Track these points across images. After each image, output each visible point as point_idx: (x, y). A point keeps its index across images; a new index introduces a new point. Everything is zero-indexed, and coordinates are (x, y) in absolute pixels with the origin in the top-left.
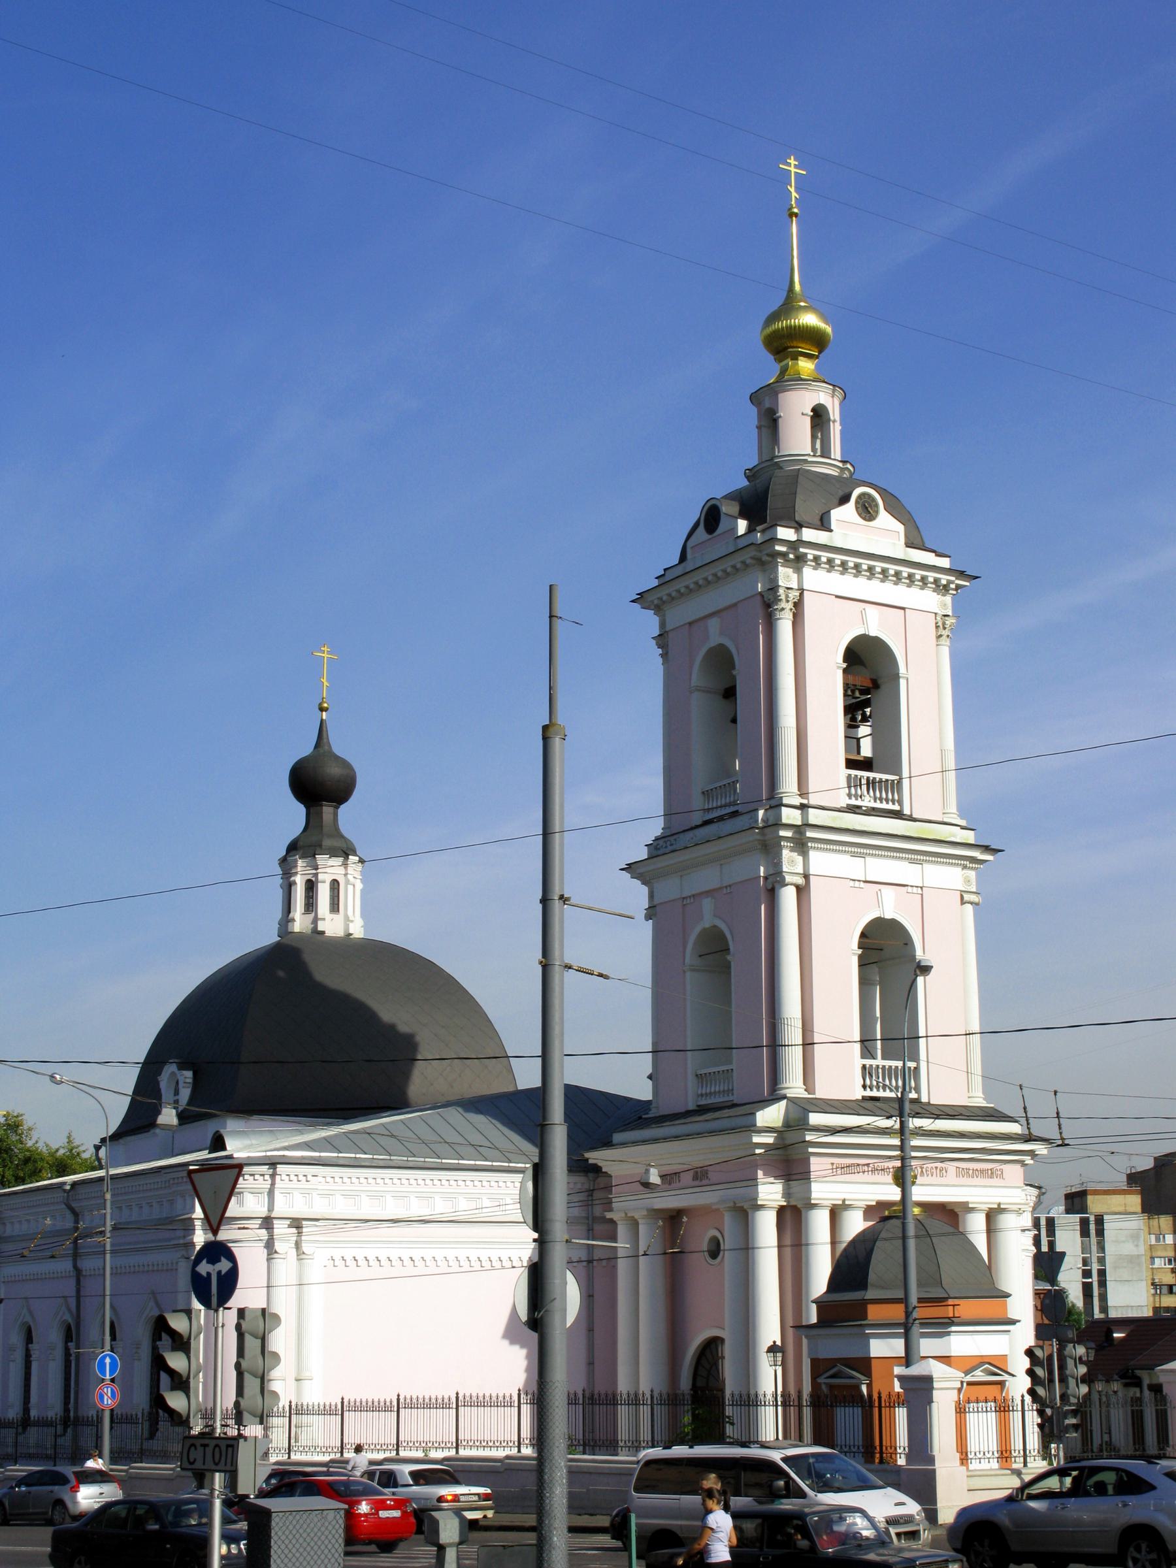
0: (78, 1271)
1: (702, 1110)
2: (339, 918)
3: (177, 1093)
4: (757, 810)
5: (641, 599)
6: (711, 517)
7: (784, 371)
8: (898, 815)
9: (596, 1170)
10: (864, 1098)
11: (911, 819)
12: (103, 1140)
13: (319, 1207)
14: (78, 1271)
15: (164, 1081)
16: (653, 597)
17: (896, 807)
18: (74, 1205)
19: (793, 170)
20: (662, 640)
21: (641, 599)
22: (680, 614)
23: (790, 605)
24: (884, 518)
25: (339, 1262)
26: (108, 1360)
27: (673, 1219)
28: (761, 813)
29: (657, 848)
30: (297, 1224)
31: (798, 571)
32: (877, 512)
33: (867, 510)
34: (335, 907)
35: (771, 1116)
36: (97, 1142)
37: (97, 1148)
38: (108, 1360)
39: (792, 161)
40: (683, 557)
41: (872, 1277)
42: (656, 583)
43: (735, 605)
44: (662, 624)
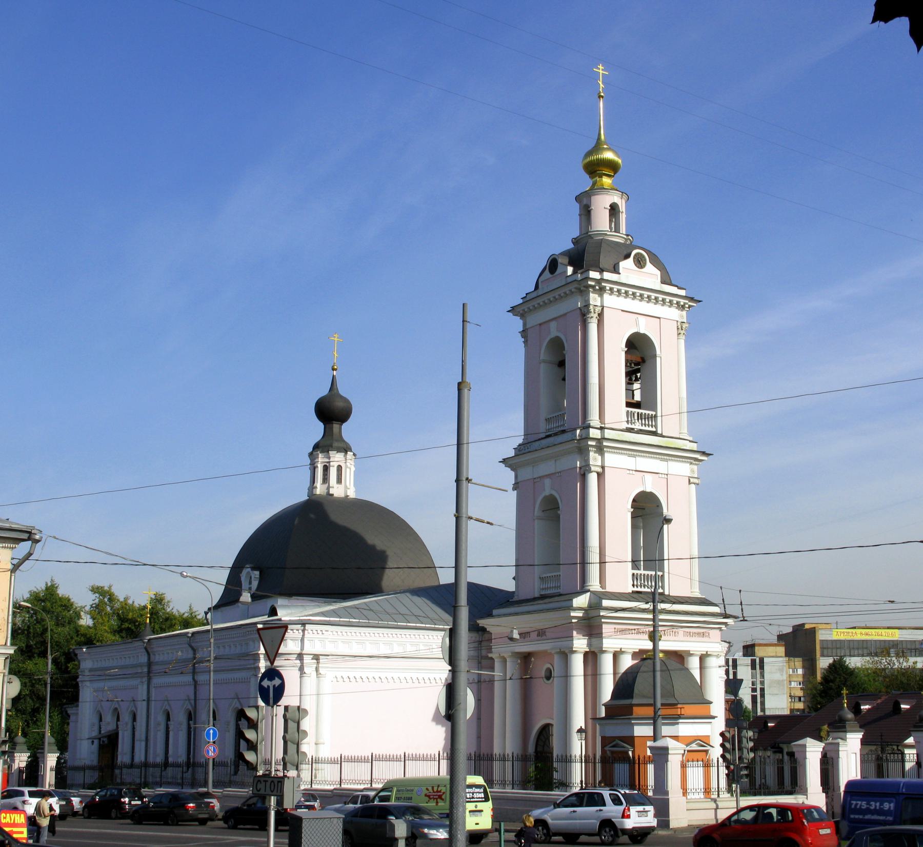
0: (196, 683)
1: (543, 597)
2: (341, 487)
3: (250, 583)
4: (575, 429)
5: (513, 310)
6: (553, 265)
7: (594, 184)
8: (654, 433)
9: (483, 630)
10: (633, 592)
11: (662, 436)
12: (209, 609)
13: (329, 649)
14: (196, 683)
15: (244, 576)
16: (520, 309)
17: (654, 429)
18: (193, 645)
19: (601, 72)
20: (524, 333)
21: (513, 310)
22: (536, 318)
23: (596, 315)
24: (649, 267)
25: (340, 679)
26: (211, 731)
27: (526, 658)
28: (578, 431)
29: (521, 450)
30: (316, 657)
31: (601, 296)
32: (645, 264)
33: (640, 262)
34: (339, 480)
35: (581, 601)
36: (206, 610)
37: (206, 613)
38: (211, 731)
39: (601, 67)
40: (537, 287)
41: (636, 691)
42: (521, 301)
43: (565, 315)
44: (525, 325)
